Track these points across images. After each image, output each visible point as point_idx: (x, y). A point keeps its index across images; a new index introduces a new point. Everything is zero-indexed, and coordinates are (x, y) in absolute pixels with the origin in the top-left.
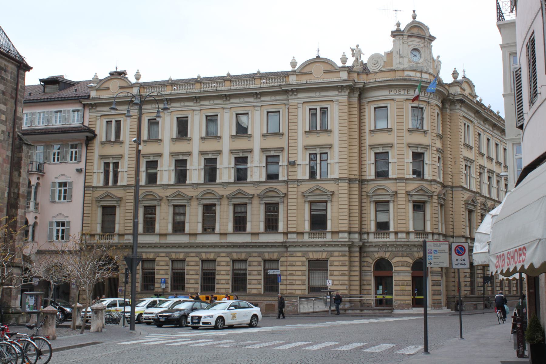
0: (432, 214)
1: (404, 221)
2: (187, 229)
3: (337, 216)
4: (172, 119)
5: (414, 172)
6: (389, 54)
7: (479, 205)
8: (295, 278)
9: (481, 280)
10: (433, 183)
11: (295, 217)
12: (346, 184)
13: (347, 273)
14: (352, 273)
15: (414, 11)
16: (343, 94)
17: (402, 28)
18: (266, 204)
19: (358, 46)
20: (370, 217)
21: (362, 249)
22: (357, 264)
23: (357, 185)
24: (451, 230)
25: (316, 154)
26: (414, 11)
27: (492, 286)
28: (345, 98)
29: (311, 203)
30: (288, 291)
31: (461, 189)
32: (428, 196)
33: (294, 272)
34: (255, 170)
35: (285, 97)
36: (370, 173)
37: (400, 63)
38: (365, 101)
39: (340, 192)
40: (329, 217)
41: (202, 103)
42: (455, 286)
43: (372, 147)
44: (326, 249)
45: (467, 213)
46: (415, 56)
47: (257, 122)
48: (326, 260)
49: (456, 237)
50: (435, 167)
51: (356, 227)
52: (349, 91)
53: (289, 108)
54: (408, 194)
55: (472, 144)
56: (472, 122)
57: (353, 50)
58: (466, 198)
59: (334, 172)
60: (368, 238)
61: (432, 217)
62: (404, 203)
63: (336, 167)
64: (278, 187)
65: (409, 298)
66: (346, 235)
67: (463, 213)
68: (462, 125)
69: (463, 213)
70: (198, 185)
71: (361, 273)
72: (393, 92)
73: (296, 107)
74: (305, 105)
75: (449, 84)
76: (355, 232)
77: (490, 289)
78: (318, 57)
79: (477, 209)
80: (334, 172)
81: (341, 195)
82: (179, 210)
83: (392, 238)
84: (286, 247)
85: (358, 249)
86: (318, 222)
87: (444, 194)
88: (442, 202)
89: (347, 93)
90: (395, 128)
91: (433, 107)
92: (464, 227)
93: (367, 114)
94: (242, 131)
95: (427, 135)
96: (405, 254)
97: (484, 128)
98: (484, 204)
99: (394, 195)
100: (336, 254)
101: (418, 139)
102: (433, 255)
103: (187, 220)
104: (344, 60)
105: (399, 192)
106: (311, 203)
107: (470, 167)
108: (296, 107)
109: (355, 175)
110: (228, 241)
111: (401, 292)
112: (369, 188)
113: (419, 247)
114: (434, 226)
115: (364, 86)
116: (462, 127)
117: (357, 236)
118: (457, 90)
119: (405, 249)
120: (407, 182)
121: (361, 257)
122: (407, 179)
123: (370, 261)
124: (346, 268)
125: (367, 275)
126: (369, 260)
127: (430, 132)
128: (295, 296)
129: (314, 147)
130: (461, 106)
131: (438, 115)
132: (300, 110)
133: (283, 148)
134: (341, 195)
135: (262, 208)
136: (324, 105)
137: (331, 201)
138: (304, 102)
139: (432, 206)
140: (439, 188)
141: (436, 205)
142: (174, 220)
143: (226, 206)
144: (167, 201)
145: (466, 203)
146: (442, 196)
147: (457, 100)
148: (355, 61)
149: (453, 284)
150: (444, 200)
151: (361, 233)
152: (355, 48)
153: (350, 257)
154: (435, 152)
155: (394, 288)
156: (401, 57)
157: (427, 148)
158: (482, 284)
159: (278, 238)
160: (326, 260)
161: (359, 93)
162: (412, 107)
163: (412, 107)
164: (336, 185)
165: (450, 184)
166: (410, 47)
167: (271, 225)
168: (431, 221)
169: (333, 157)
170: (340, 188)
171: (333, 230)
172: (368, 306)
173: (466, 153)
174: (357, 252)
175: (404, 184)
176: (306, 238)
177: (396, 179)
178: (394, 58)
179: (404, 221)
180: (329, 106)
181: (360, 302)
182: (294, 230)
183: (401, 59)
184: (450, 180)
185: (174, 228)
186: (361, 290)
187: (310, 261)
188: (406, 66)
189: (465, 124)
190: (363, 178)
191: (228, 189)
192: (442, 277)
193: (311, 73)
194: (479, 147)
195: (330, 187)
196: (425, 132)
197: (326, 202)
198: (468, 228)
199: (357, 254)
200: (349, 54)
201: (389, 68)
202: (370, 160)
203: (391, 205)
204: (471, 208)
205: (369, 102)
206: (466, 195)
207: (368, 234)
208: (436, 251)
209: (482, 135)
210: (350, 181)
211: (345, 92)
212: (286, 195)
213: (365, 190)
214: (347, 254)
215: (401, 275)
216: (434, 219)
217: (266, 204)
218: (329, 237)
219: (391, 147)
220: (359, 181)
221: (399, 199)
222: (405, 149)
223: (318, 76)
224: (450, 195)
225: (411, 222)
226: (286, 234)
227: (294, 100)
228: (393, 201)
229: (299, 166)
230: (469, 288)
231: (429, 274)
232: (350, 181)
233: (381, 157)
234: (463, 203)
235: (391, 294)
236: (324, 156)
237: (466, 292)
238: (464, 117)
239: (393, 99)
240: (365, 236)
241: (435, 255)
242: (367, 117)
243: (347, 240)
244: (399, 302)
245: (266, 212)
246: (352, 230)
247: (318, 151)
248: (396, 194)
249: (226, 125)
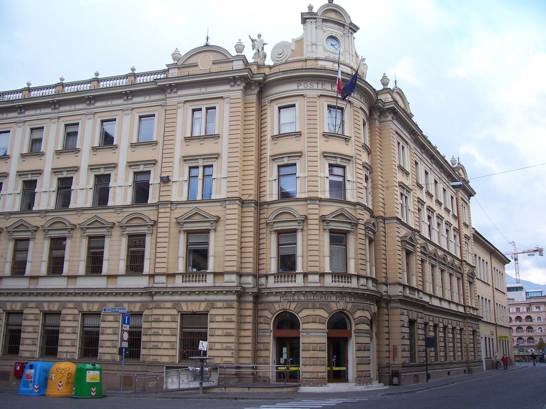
0: (356, 249)
1: (317, 258)
2: (28, 272)
3: (222, 250)
4: (24, 131)
6: (299, 42)
7: (419, 246)
9: (423, 343)
10: (358, 207)
11: (167, 253)
12: (236, 206)
13: (233, 332)
14: (243, 333)
16: (236, 88)
17: (315, 10)
18: (130, 236)
19: (259, 36)
20: (270, 254)
21: (258, 296)
22: (250, 319)
23: (252, 209)
24: (384, 275)
27: (436, 351)
28: (239, 94)
29: (189, 233)
30: (152, 357)
31: (396, 221)
32: (350, 223)
33: (160, 331)
34: (118, 190)
35: (161, 97)
38: (266, 100)
39: (228, 217)
40: (211, 252)
41: (62, 109)
42: (389, 351)
43: (275, 158)
44: (202, 297)
47: (125, 130)
48: (205, 314)
49: (390, 284)
50: (361, 186)
51: (249, 268)
52: (244, 84)
53: (166, 110)
54: (323, 219)
55: (408, 168)
56: (407, 143)
57: (253, 41)
58: (402, 235)
59: (220, 191)
60: (267, 284)
61: (356, 254)
62: (317, 232)
63: (224, 183)
64: (146, 213)
65: (323, 370)
66: (234, 278)
67: (400, 253)
68: (396, 144)
69: (400, 253)
70: (47, 211)
71: (256, 331)
72: (302, 85)
73: (175, 107)
74: (187, 105)
76: (248, 275)
77: (433, 354)
78: (207, 45)
79: (416, 251)
80: (220, 191)
81: (228, 222)
82: (21, 245)
83: (299, 281)
84: (151, 294)
85: (251, 299)
86: (198, 257)
87: (373, 224)
88: (371, 234)
89: (241, 87)
90: (305, 132)
91: (357, 110)
92: (401, 271)
93: (268, 116)
94: (107, 140)
95: (350, 143)
96: (318, 305)
97: (421, 157)
98: (424, 247)
99: (303, 221)
100: (220, 305)
103: (29, 258)
104: (240, 48)
105: (310, 217)
106: (189, 233)
108: (175, 107)
109: (250, 195)
110: (76, 287)
111: (311, 361)
112: (269, 213)
113: (338, 295)
114: (361, 267)
115: (265, 79)
116: (396, 148)
117: (250, 279)
118: (387, 98)
119: (317, 298)
120: (322, 203)
121: (256, 310)
122: (321, 200)
123: (269, 315)
125: (264, 336)
126: (267, 314)
127: (353, 139)
128: (159, 365)
129: (195, 158)
130: (392, 118)
131: (364, 125)
132: (180, 112)
133: (156, 161)
134: (228, 222)
135: (124, 241)
136: (210, 104)
137: (215, 230)
139: (356, 239)
140: (366, 217)
141: (363, 237)
142: (14, 258)
143: (78, 240)
144: (7, 234)
145: (403, 241)
146: (371, 226)
148: (256, 54)
149: (387, 348)
150: (374, 233)
151: (257, 276)
152: (257, 38)
153: (240, 309)
154: (361, 167)
155: (302, 354)
157: (349, 160)
158: (424, 347)
160: (205, 314)
161: (258, 89)
162: (329, 106)
164: (222, 208)
165: (382, 214)
166: (326, 34)
167: (135, 264)
168: (356, 259)
169: (220, 171)
170: (228, 212)
171: (216, 271)
172: (265, 381)
173: (400, 177)
174: (249, 302)
175: (317, 206)
176: (178, 282)
177: (306, 200)
179: (317, 258)
180: (217, 104)
181: (253, 374)
182: (163, 271)
184: (382, 209)
185: (13, 268)
186: (255, 358)
187: (183, 315)
189: (399, 143)
190: (263, 200)
191: (82, 216)
192: (371, 339)
193: (197, 66)
195: (213, 210)
196: (347, 139)
197: (207, 232)
198: (406, 273)
199: (250, 306)
200: (248, 44)
201: (299, 58)
202: (271, 175)
203: (299, 235)
204: (410, 248)
205: (272, 101)
206: (404, 231)
207: (267, 276)
210: (243, 203)
211: (239, 85)
212: (155, 223)
213: (265, 216)
214: (235, 304)
215: (311, 336)
216: (360, 256)
217: (130, 236)
218: (210, 281)
219: (300, 156)
220: (256, 203)
221: (310, 227)
222: (318, 159)
223: (205, 64)
224: (382, 229)
225: (327, 260)
226: (152, 276)
227: (173, 99)
228: (302, 230)
229: (175, 183)
230: (408, 354)
231: (353, 335)
232: (243, 203)
234: (400, 240)
236: (208, 171)
237: (404, 359)
238: (397, 132)
239: (302, 95)
240: (263, 281)
242: (269, 120)
243: (235, 284)
247: (201, 163)
248: (305, 219)
249: (89, 135)
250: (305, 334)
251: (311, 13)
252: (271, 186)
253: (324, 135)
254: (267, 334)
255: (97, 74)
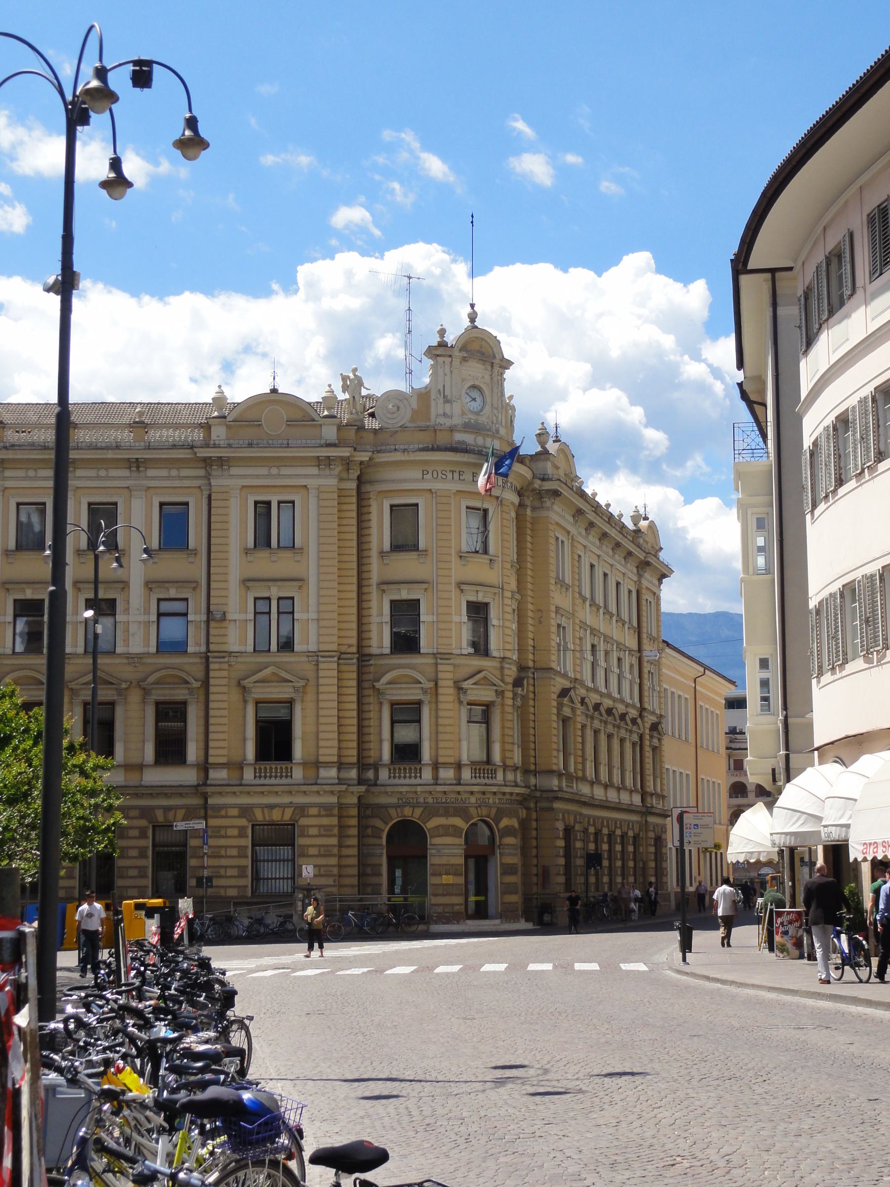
5: (474, 645)
6: (424, 395)
8: (224, 862)
11: (228, 732)
14: (345, 852)
15: (472, 306)
25: (269, 599)
26: (472, 306)
36: (381, 638)
37: (445, 415)
43: (385, 584)
45: (561, 723)
46: (474, 399)
49: (541, 772)
51: (352, 755)
59: (306, 640)
75: (531, 456)
76: (350, 765)
78: (274, 391)
86: (275, 740)
101: (478, 570)
102: (693, 831)
107: (564, 628)
109: (350, 646)
124: (334, 841)
138: (243, 487)
147: (548, 491)
156: (447, 401)
159: (186, 776)
162: (468, 508)
163: (468, 508)
167: (170, 749)
178: (433, 403)
182: (224, 760)
183: (447, 405)
188: (457, 421)
194: (580, 587)
208: (697, 825)
209: (596, 567)
233: (406, 613)
235: (424, 893)
241: (696, 831)
242: (374, 524)
244: (440, 910)
245: (157, 720)
246: (344, 760)
250: (434, 851)
251: (442, 345)
252: (381, 632)
253: (461, 557)
254: (379, 851)
255: (726, 941)
